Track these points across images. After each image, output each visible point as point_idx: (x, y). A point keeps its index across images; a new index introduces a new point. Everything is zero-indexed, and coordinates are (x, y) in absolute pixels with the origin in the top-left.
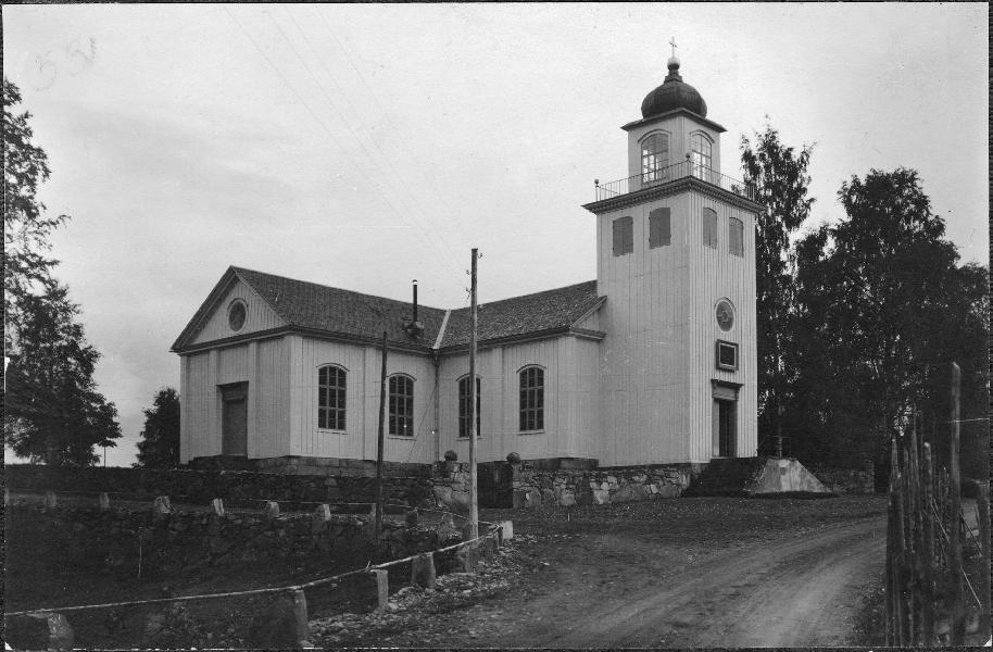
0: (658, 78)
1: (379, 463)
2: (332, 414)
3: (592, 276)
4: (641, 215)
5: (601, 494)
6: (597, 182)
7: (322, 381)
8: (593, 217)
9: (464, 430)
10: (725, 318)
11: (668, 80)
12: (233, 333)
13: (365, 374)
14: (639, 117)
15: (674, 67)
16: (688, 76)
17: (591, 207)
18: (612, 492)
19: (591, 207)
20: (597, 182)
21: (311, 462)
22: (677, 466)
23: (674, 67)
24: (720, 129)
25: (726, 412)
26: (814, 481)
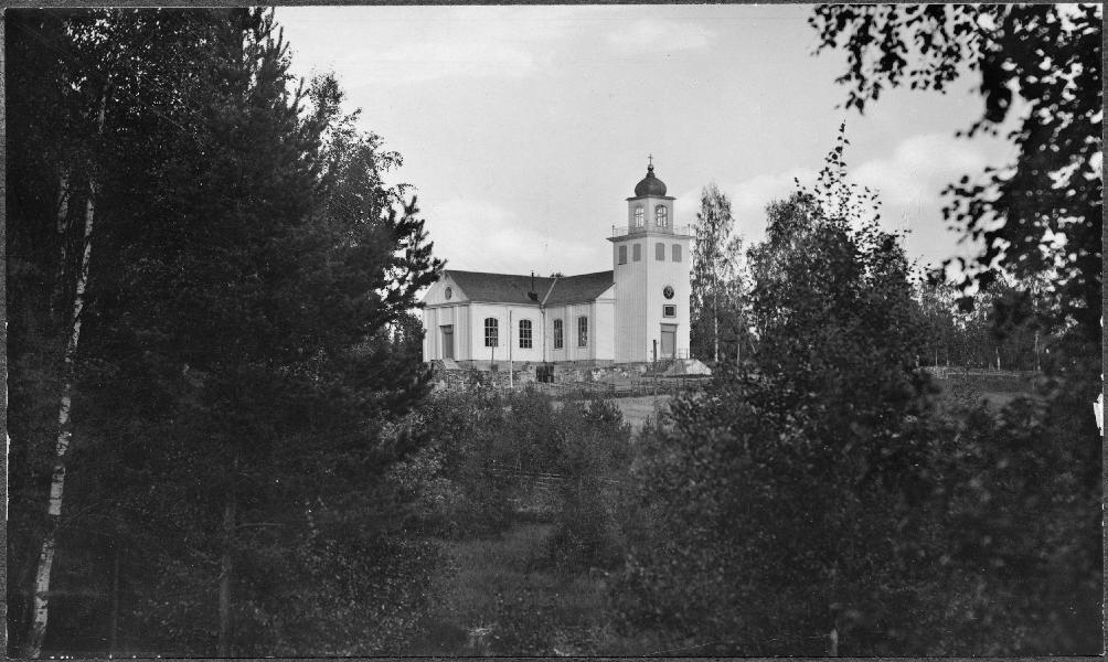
0: (643, 175)
1: (544, 362)
2: (526, 341)
3: (609, 267)
4: (630, 245)
5: (596, 376)
6: (359, 111)
7: (521, 326)
8: (612, 243)
9: (582, 343)
10: (669, 293)
11: (648, 175)
12: (445, 301)
13: (509, 316)
14: (634, 195)
15: (650, 169)
16: (658, 174)
17: (611, 239)
18: (602, 376)
19: (611, 239)
20: (359, 111)
21: (616, 347)
22: (642, 363)
23: (650, 169)
24: (673, 199)
25: (669, 331)
26: (704, 366)
